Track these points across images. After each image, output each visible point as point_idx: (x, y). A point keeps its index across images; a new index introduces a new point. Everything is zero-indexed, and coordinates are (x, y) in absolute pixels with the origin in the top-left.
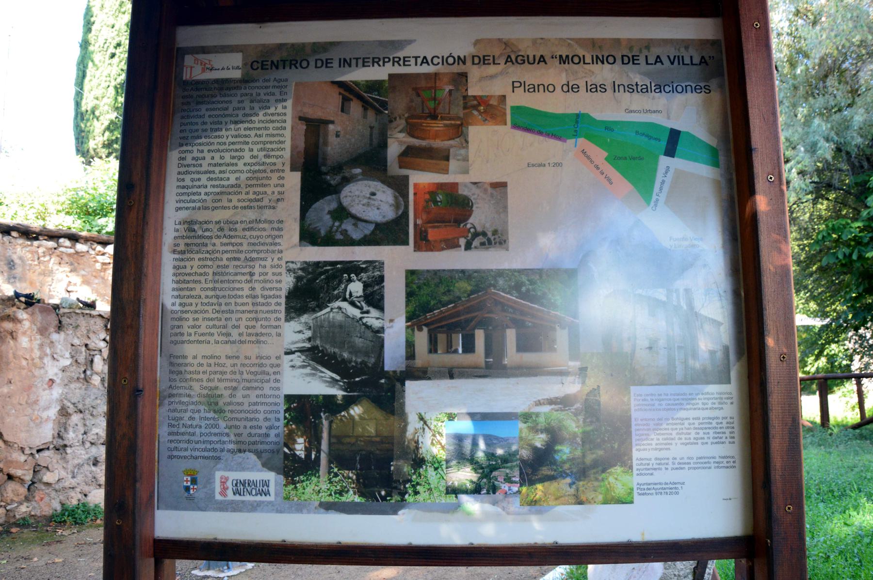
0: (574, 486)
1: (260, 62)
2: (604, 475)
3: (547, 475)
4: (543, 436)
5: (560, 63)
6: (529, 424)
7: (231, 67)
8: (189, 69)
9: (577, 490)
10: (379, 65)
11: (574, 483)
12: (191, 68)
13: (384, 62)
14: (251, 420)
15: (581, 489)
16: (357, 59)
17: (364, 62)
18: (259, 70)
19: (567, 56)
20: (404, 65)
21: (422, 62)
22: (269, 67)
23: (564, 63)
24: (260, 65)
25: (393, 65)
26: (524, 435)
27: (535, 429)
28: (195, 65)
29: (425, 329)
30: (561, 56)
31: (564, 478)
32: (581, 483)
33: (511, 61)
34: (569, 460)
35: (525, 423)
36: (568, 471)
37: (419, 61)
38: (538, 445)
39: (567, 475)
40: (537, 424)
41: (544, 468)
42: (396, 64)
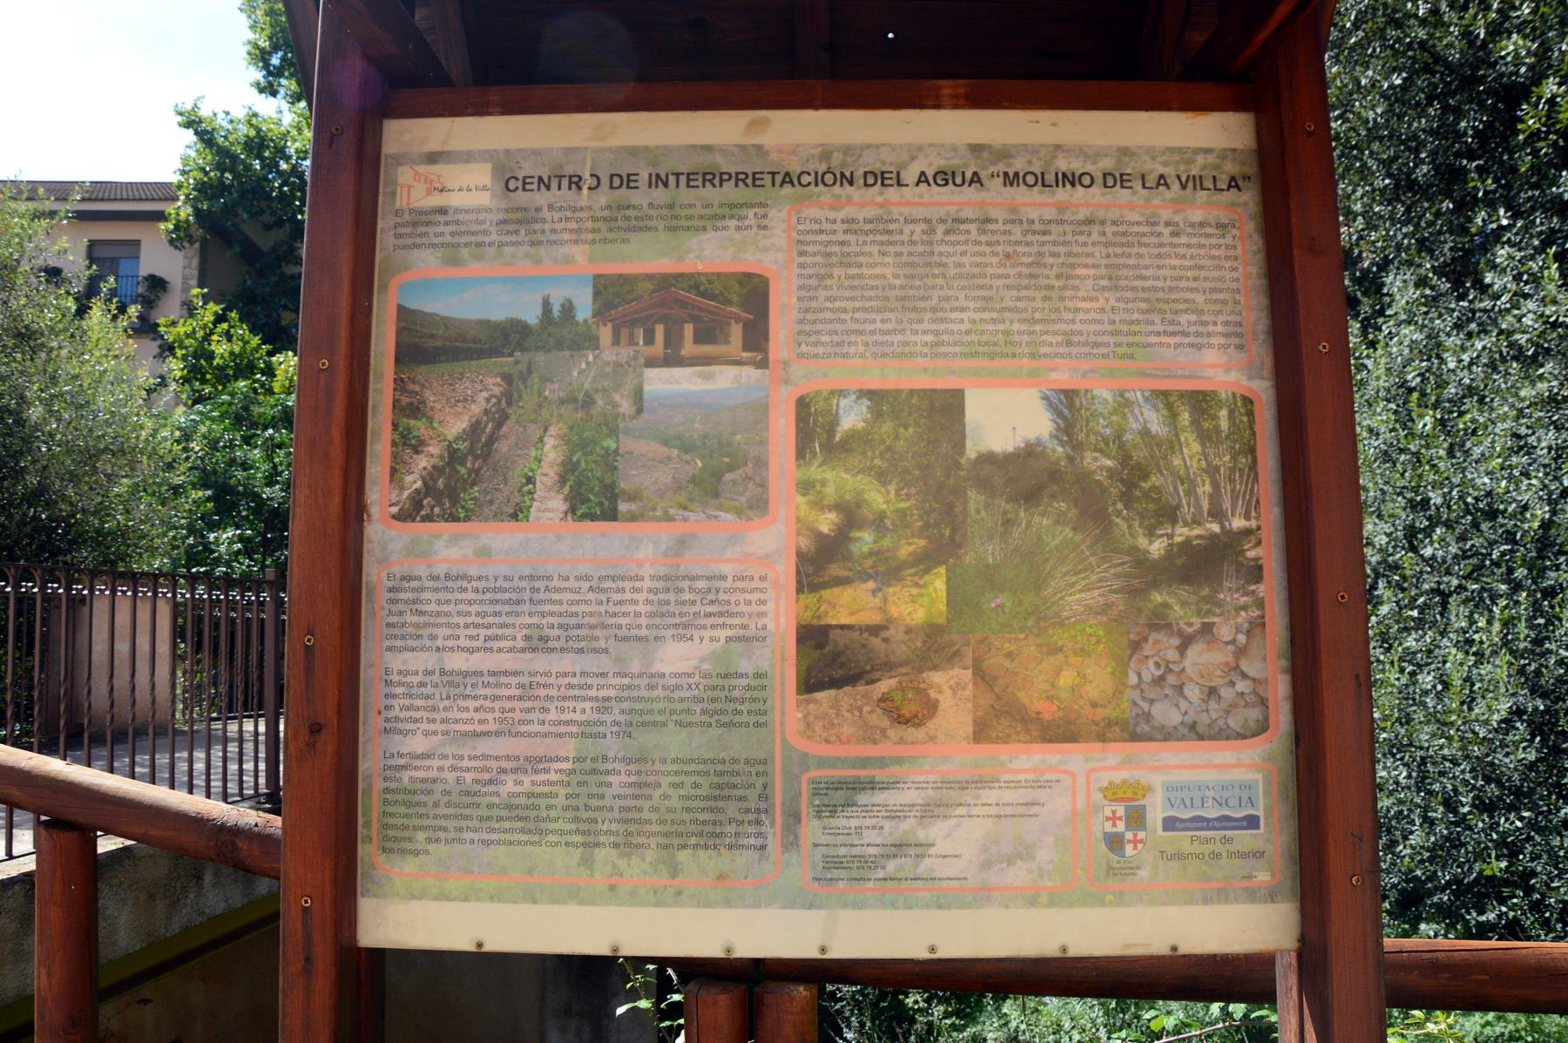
0: (880, 594)
1: (520, 178)
2: (927, 578)
3: (837, 577)
4: (832, 516)
5: (1005, 185)
6: (810, 497)
7: (473, 187)
8: (405, 190)
9: (885, 600)
10: (714, 186)
11: (880, 589)
12: (410, 187)
13: (722, 181)
14: (642, 713)
15: (891, 599)
16: (678, 175)
17: (689, 180)
18: (520, 192)
19: (1016, 174)
20: (754, 186)
21: (783, 182)
22: (535, 186)
23: (1011, 184)
24: (520, 184)
25: (737, 185)
26: (802, 514)
27: (818, 505)
28: (415, 184)
29: (609, 325)
30: (1006, 174)
31: (865, 581)
32: (891, 590)
33: (927, 181)
34: (873, 553)
35: (804, 495)
36: (870, 571)
37: (779, 179)
38: (825, 529)
39: (870, 577)
40: (823, 497)
41: (833, 566)
42: (740, 183)
